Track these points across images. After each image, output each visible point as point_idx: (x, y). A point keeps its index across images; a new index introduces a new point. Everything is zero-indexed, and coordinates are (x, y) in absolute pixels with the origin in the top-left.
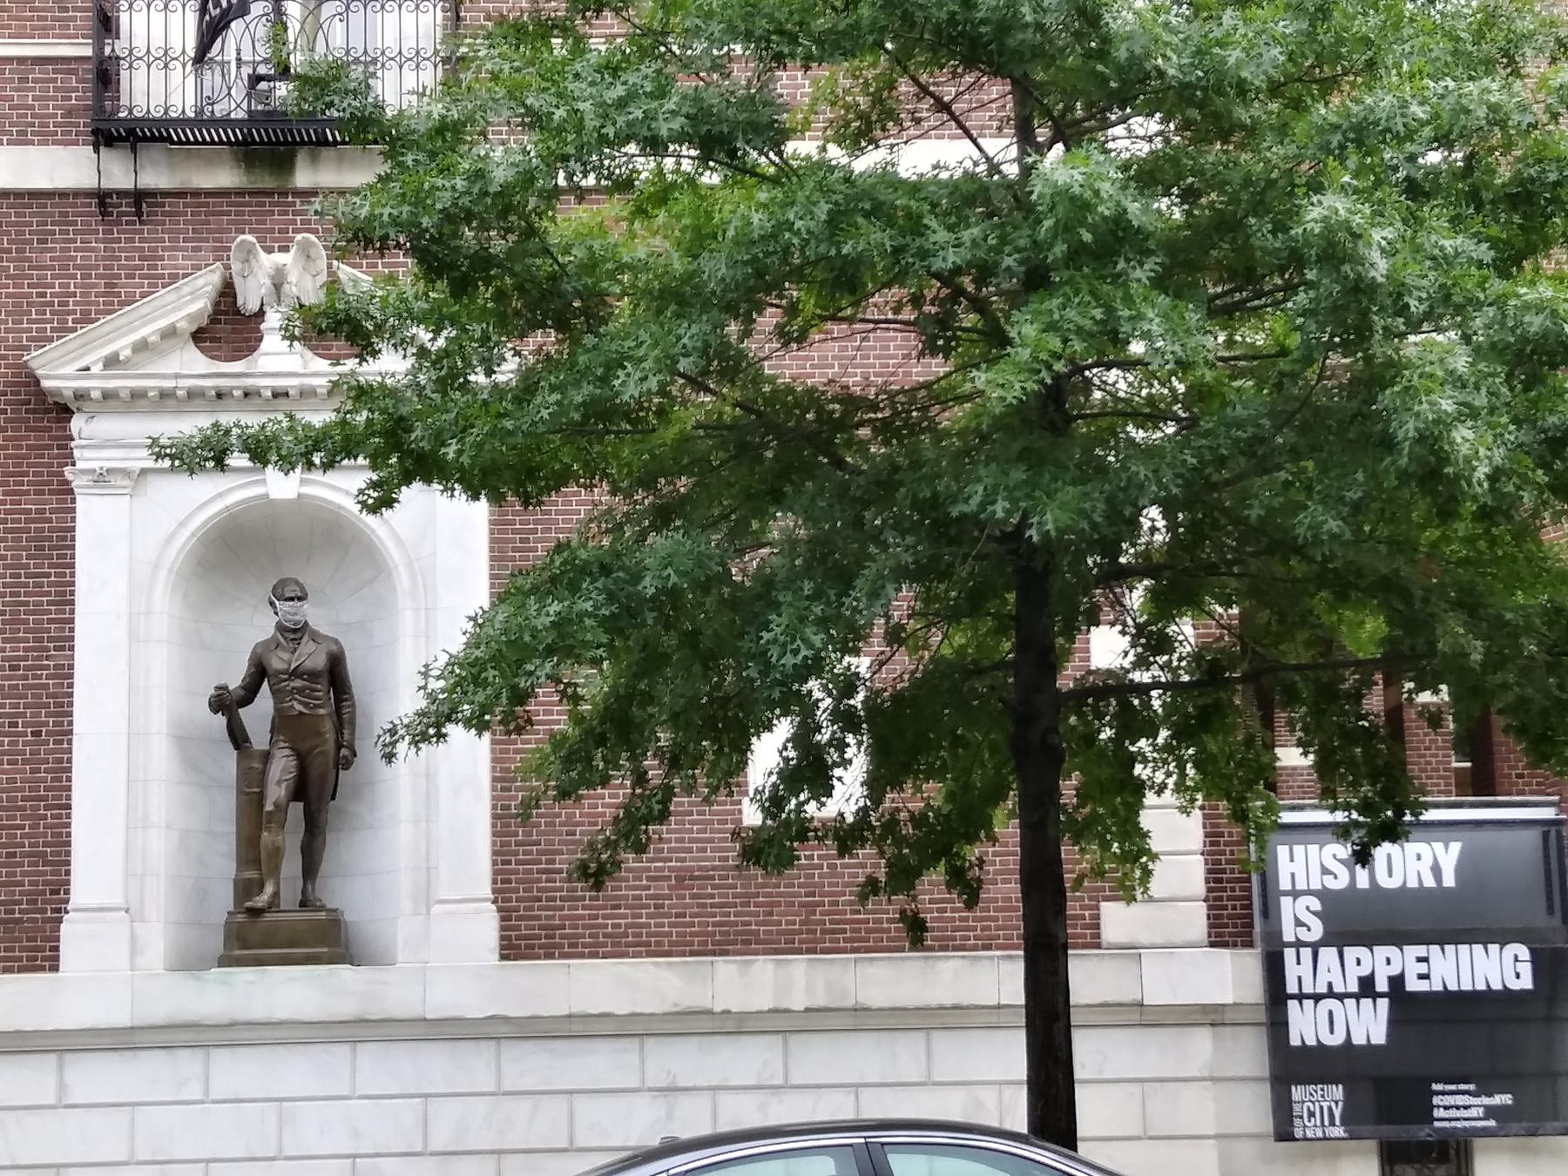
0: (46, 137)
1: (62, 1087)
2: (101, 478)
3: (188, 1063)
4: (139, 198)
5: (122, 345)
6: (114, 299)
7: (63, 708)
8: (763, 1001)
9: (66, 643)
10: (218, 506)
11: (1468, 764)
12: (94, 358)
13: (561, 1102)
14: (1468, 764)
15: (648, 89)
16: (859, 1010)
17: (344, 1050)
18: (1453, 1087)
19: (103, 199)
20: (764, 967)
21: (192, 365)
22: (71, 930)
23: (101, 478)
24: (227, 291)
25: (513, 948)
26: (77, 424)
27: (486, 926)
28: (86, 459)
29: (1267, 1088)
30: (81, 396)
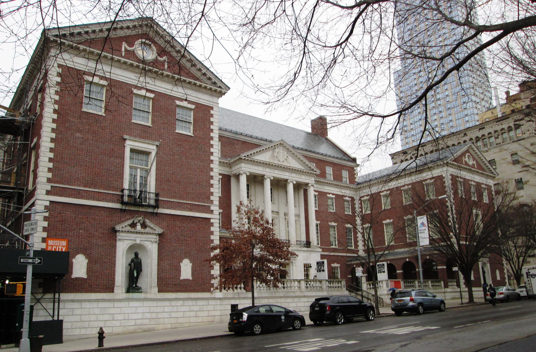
0: (115, 202)
1: (114, 305)
2: (120, 240)
3: (127, 303)
4: (125, 210)
5: (124, 226)
6: (123, 222)
7: (114, 264)
8: (182, 297)
9: (115, 257)
10: (131, 244)
11: (445, 267)
12: (121, 227)
13: (163, 307)
14: (445, 267)
15: (318, 173)
16: (191, 298)
17: (142, 302)
18: (432, 311)
19: (121, 210)
20: (183, 294)
21: (129, 228)
22: (115, 288)
23: (120, 240)
24: (133, 221)
25: (159, 291)
26: (117, 234)
27: (157, 289)
28: (118, 238)
29: (99, 303)
30: (119, 231)
